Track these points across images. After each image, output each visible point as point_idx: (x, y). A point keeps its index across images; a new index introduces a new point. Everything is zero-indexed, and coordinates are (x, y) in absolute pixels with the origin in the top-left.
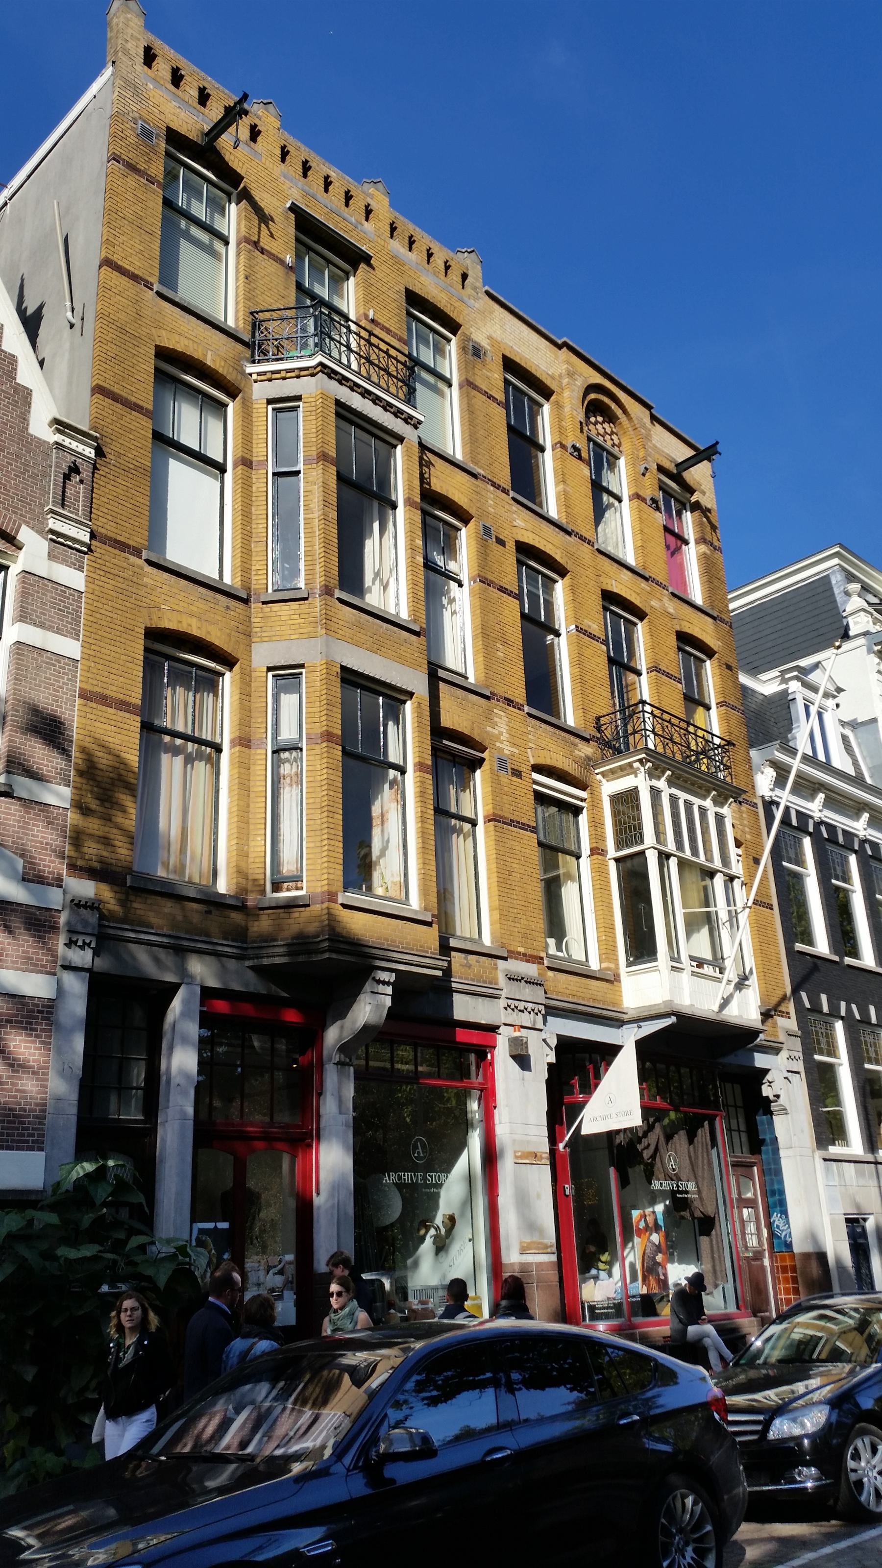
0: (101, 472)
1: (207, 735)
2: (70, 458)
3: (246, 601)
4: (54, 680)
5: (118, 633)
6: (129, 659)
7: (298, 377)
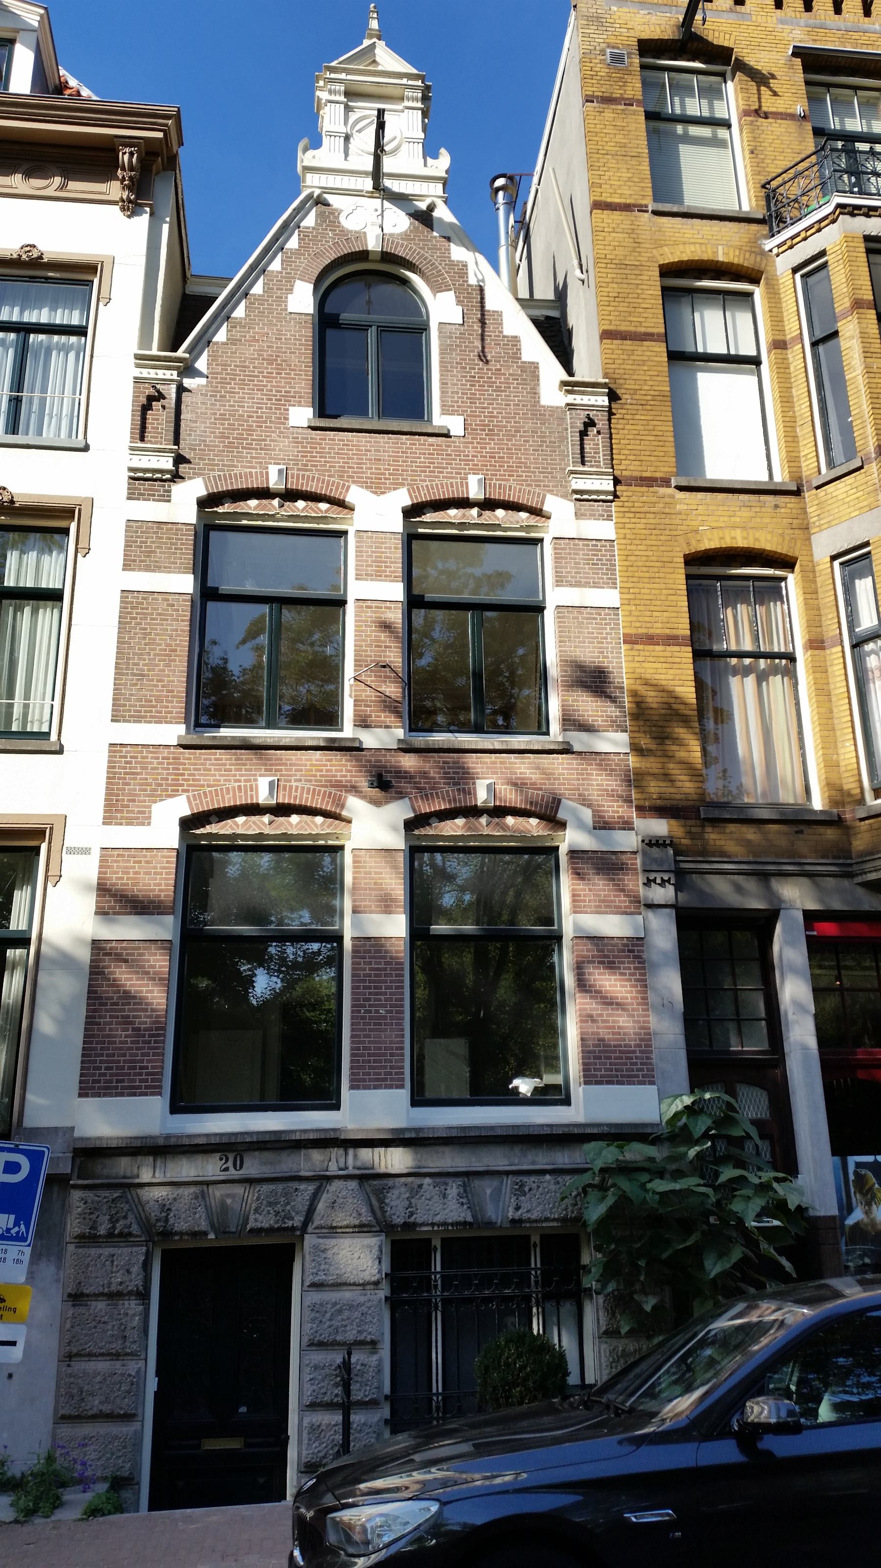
0: (618, 416)
1: (778, 647)
3: (797, 493)
4: (597, 633)
7: (819, 230)
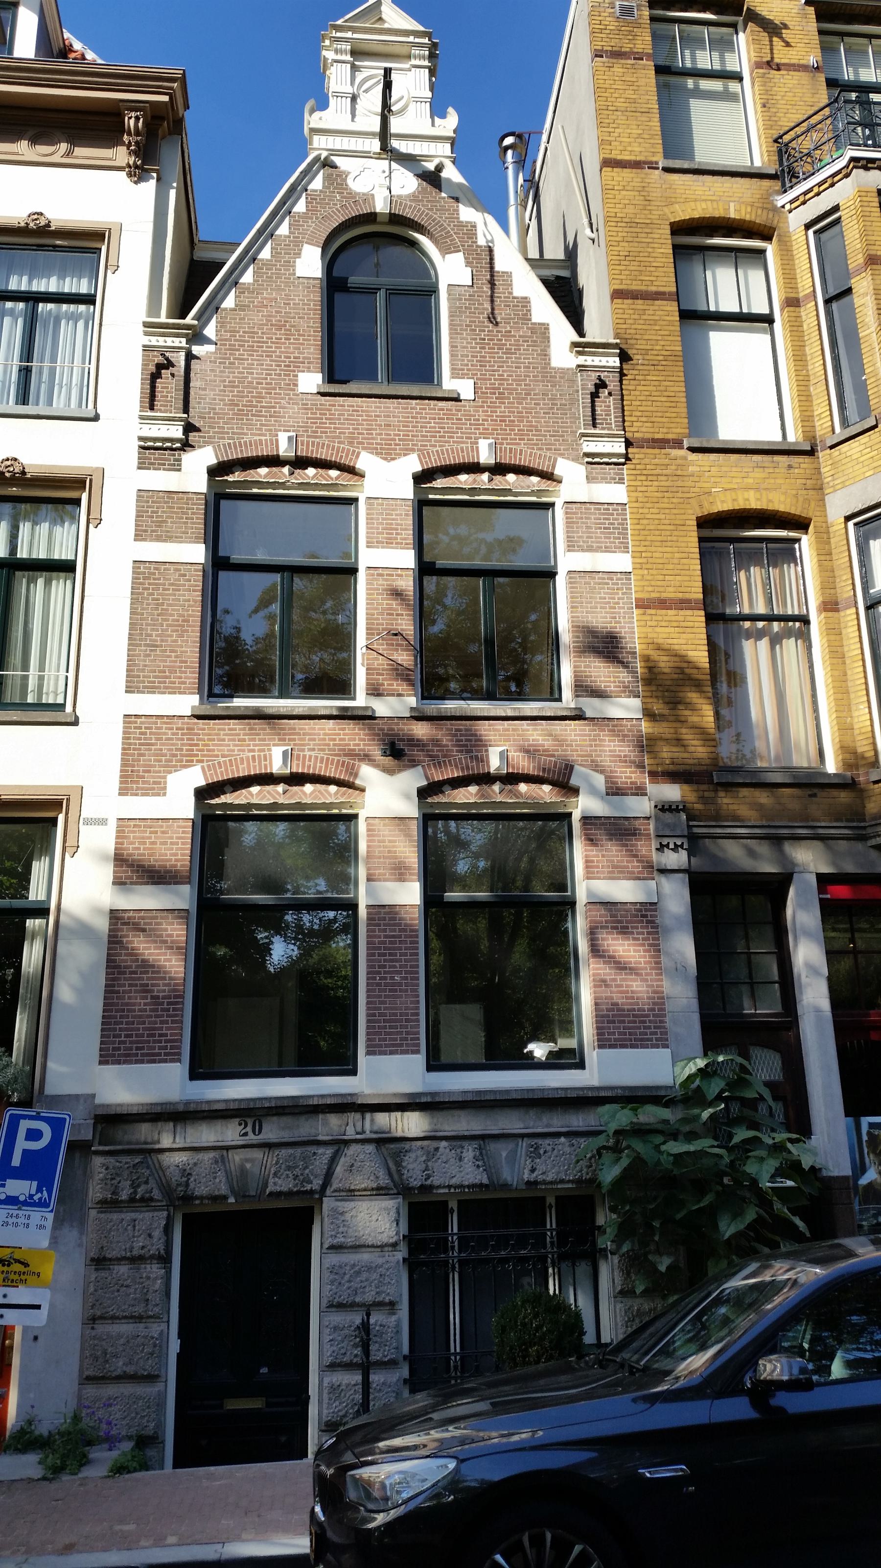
0: (629, 377)
1: (792, 609)
2: (594, 376)
3: (811, 452)
4: (609, 598)
5: (668, 533)
6: (684, 555)
